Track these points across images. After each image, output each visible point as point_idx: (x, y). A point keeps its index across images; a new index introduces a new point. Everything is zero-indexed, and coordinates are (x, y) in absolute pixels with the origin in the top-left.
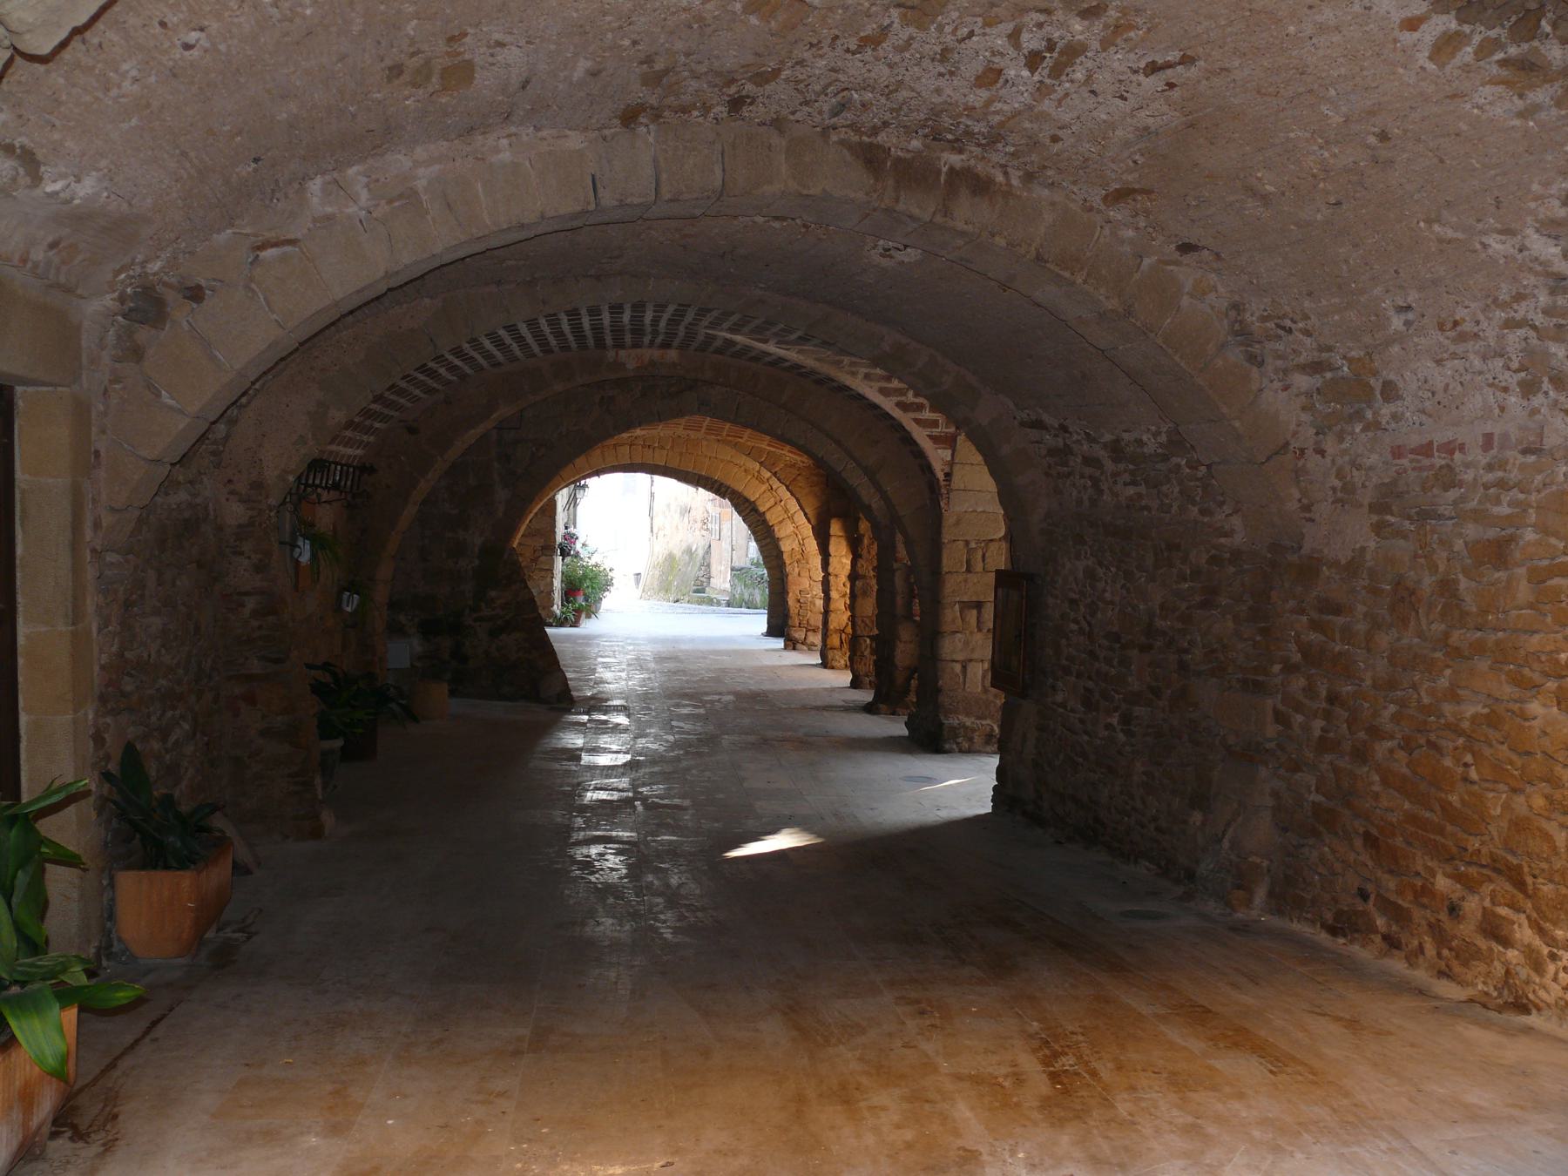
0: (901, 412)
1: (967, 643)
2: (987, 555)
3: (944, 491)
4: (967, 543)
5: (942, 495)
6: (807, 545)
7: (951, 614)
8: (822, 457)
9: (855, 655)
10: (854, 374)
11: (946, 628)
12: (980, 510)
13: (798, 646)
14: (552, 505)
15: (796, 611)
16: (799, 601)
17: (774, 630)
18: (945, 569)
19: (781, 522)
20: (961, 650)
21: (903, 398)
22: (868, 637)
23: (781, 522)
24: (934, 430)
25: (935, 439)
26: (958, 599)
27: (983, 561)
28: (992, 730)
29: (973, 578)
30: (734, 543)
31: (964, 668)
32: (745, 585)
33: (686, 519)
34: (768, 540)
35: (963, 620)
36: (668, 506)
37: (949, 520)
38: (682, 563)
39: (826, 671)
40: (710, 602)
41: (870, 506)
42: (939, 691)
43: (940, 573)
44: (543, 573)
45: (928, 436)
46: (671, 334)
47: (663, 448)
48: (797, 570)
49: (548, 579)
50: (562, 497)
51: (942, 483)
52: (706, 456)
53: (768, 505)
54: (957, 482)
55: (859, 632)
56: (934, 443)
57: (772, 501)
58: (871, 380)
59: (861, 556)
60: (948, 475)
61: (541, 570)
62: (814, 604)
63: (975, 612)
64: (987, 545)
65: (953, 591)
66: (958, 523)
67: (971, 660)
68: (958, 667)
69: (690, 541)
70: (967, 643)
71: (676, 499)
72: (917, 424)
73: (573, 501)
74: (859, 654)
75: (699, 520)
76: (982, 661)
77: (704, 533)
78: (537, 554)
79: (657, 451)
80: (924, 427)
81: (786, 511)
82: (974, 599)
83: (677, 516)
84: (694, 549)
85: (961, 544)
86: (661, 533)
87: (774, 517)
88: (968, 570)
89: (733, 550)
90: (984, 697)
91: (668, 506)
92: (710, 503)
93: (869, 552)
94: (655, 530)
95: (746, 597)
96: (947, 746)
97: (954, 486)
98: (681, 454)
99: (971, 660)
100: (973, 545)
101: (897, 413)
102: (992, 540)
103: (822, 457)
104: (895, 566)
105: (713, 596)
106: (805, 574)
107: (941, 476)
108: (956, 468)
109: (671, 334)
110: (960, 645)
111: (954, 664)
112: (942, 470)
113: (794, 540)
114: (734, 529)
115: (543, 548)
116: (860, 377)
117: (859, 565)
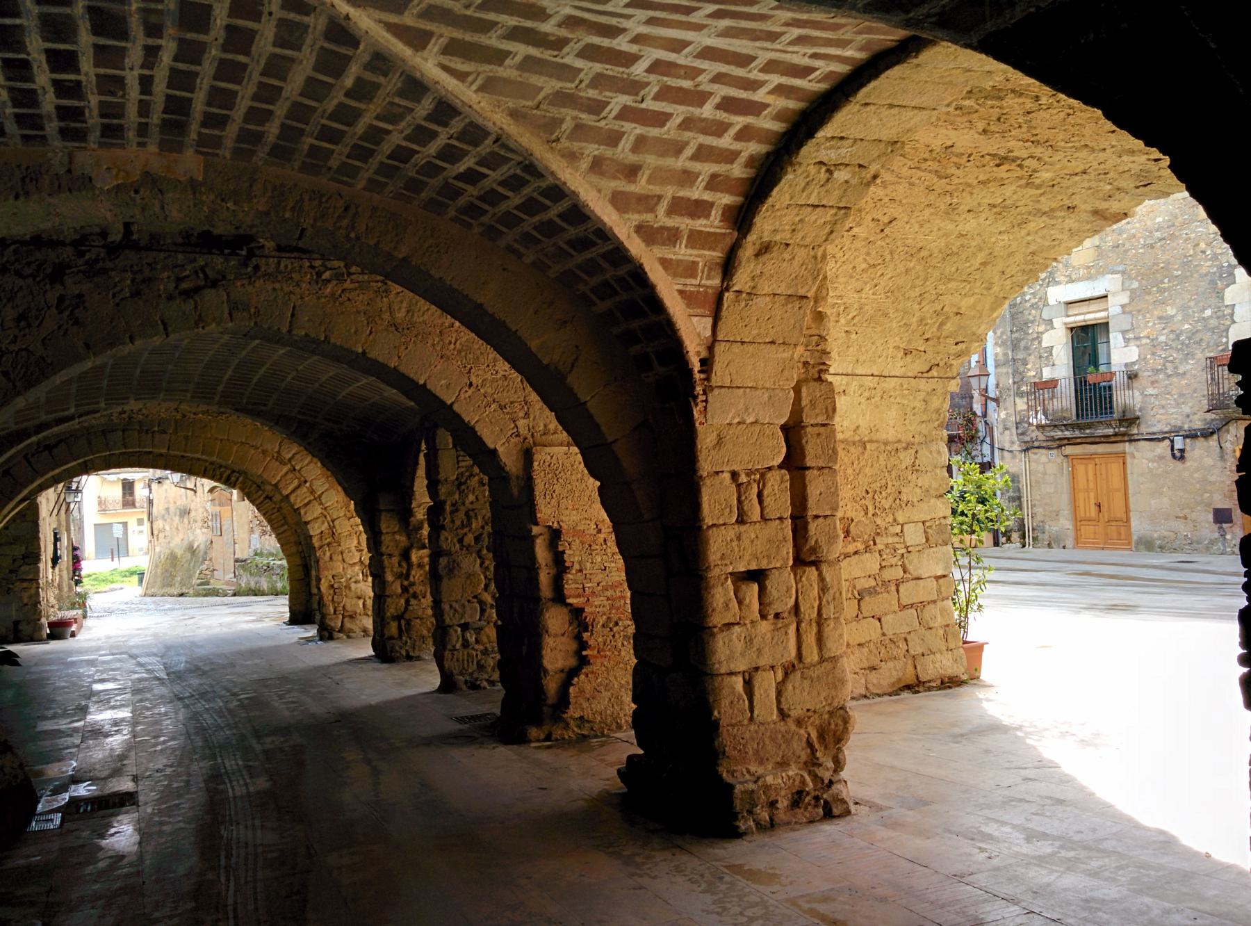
0: (643, 245)
1: (749, 641)
2: (765, 493)
3: (699, 389)
4: (734, 475)
5: (695, 397)
6: (337, 527)
7: (721, 596)
8: (425, 385)
9: (444, 648)
10: (572, 157)
11: (717, 620)
12: (750, 420)
13: (336, 635)
14: (35, 509)
15: (330, 598)
16: (332, 586)
17: (298, 617)
18: (708, 521)
19: (306, 505)
20: (742, 654)
21: (648, 217)
22: (459, 625)
23: (306, 505)
24: (689, 281)
25: (688, 297)
26: (730, 569)
27: (761, 502)
28: (803, 782)
29: (749, 531)
30: (236, 537)
31: (748, 685)
32: (251, 574)
33: (186, 521)
34: (286, 527)
35: (740, 602)
36: (167, 509)
37: (706, 439)
38: (184, 560)
39: (331, 644)
40: (215, 593)
41: (495, 450)
42: (715, 726)
43: (700, 528)
44: (25, 585)
45: (681, 292)
46: (178, 107)
47: (164, 432)
48: (328, 554)
49: (33, 591)
50: (47, 500)
51: (697, 376)
52: (216, 439)
53: (291, 488)
54: (720, 374)
55: (448, 621)
56: (688, 306)
57: (296, 483)
58: (602, 174)
59: (443, 527)
60: (707, 364)
61: (23, 580)
62: (350, 589)
63: (756, 587)
64: (763, 475)
65: (723, 557)
66: (720, 441)
67: (757, 669)
68: (738, 683)
69: (191, 539)
70: (749, 641)
71: (175, 503)
72: (665, 269)
73: (64, 507)
74: (449, 647)
75: (199, 519)
76: (772, 667)
77: (204, 530)
78: (17, 564)
79: (157, 436)
80: (675, 275)
81: (312, 492)
82: (753, 567)
83: (177, 519)
84: (195, 547)
85: (727, 476)
86: (161, 535)
87: (298, 501)
88: (741, 520)
89: (235, 543)
90: (782, 727)
91: (167, 509)
92: (209, 504)
93: (453, 521)
94: (155, 532)
95: (253, 585)
96: (742, 826)
97: (715, 380)
98: (186, 438)
99: (757, 669)
100: (743, 478)
101: (636, 247)
102: (770, 469)
103: (425, 385)
104: (535, 530)
105: (218, 587)
106: (338, 558)
107: (696, 366)
108: (719, 348)
109: (178, 107)
110: (739, 646)
111: (734, 678)
112: (698, 353)
113: (323, 523)
114: (235, 524)
115: (24, 557)
116: (584, 165)
117: (442, 538)
